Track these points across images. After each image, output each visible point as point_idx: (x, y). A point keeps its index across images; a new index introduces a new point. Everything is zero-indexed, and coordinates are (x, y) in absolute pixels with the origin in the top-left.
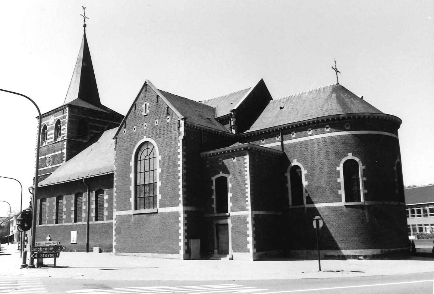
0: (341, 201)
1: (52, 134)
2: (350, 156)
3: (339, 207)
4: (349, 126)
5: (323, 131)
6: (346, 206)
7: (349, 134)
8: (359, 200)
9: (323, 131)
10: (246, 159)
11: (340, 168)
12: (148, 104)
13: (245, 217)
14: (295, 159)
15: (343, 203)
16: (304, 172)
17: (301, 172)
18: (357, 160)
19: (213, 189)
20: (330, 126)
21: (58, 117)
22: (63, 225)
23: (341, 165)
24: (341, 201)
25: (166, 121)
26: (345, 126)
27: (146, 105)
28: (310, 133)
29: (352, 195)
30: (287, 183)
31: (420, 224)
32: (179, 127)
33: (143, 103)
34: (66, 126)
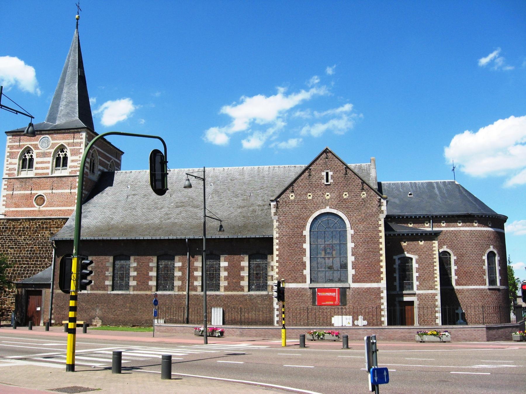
0: (485, 285)
1: (77, 167)
2: (491, 249)
3: (484, 290)
4: (491, 223)
5: (472, 225)
6: (489, 289)
7: (493, 230)
8: (496, 285)
9: (472, 225)
10: (434, 243)
11: (485, 258)
12: (330, 174)
13: (435, 295)
14: (444, 245)
15: (487, 287)
16: (453, 258)
17: (450, 258)
18: (496, 252)
19: (395, 268)
20: (478, 222)
21: (62, 142)
22: (130, 294)
23: (486, 255)
24: (485, 285)
25: (361, 197)
26: (489, 224)
27: (327, 174)
28: (459, 225)
29: (492, 282)
30: (500, 270)
31: (285, 306)
32: (380, 206)
33: (322, 171)
34: (80, 157)
